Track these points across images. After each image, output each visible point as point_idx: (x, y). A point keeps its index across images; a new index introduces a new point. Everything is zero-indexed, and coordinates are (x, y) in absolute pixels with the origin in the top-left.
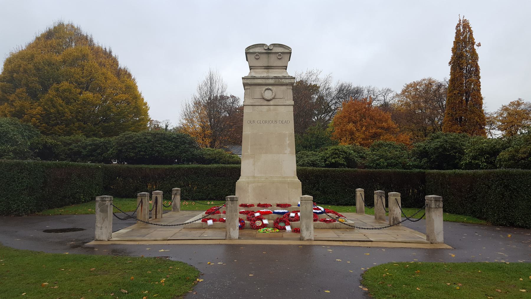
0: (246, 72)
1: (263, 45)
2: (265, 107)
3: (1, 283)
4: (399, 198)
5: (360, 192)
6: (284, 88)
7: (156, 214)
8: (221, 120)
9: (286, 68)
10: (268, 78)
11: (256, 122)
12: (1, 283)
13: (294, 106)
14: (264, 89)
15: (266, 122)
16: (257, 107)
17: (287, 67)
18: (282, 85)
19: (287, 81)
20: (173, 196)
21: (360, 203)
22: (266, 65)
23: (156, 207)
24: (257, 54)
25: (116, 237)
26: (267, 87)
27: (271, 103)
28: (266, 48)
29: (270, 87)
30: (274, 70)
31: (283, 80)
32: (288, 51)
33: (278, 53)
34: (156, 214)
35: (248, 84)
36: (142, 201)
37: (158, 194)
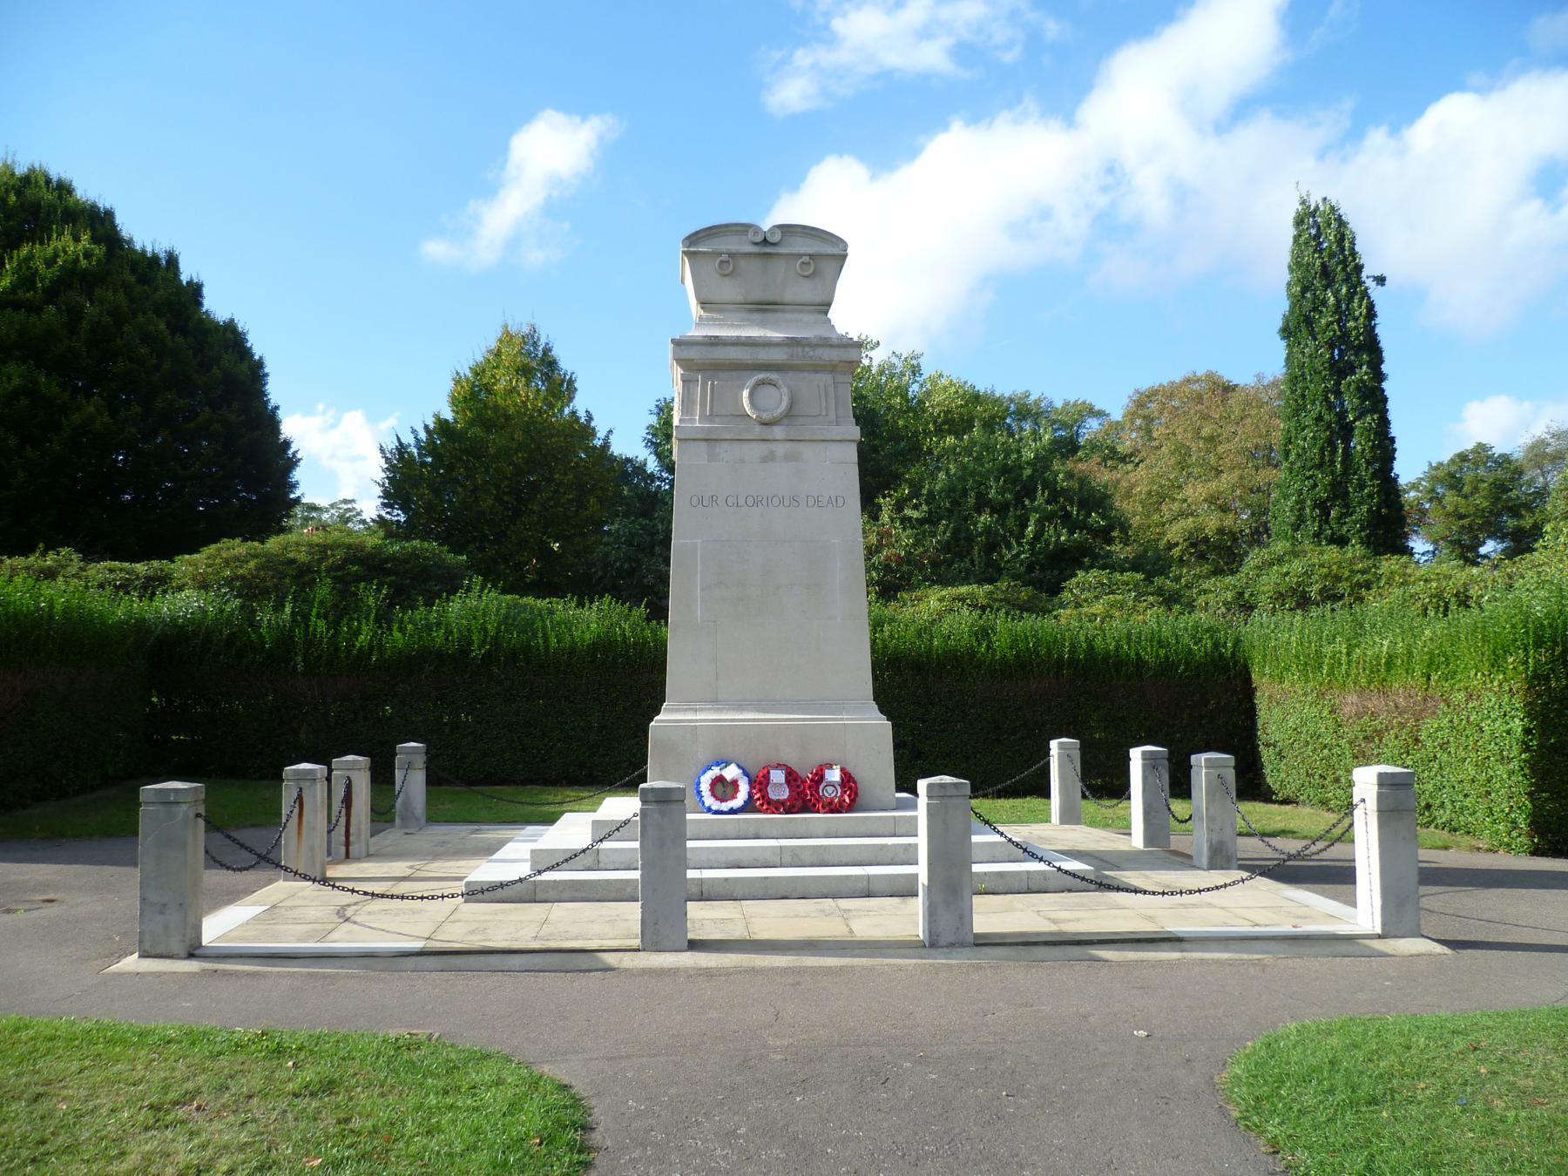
0: (691, 320)
1: (744, 229)
2: (754, 445)
3: (1564, 1112)
4: (1230, 775)
5: (1060, 752)
6: (825, 378)
7: (347, 844)
8: (514, 480)
9: (826, 306)
10: (767, 344)
12: (1564, 1112)
13: (860, 445)
14: (752, 381)
15: (756, 503)
16: (725, 445)
17: (829, 305)
18: (817, 368)
19: (827, 355)
20: (398, 774)
22: (758, 295)
23: (348, 815)
24: (725, 257)
25: (1098, 960)
26: (761, 376)
27: (778, 432)
28: (759, 238)
29: (773, 376)
30: (787, 316)
31: (819, 352)
32: (835, 251)
33: (801, 255)
34: (347, 844)
35: (702, 362)
36: (300, 799)
37: (353, 767)
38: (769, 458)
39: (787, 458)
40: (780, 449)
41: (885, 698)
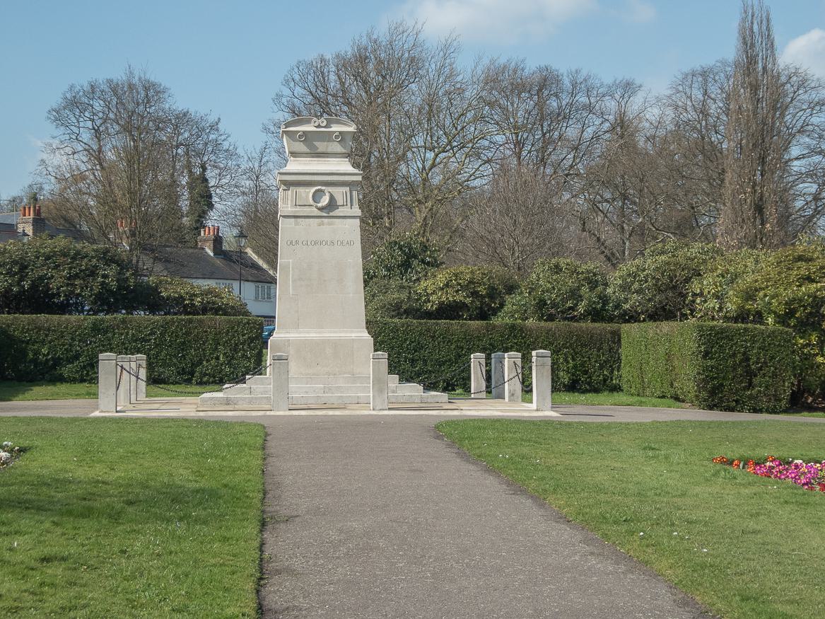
5: (476, 360)
11: (300, 243)
38: (323, 224)
41: (370, 325)
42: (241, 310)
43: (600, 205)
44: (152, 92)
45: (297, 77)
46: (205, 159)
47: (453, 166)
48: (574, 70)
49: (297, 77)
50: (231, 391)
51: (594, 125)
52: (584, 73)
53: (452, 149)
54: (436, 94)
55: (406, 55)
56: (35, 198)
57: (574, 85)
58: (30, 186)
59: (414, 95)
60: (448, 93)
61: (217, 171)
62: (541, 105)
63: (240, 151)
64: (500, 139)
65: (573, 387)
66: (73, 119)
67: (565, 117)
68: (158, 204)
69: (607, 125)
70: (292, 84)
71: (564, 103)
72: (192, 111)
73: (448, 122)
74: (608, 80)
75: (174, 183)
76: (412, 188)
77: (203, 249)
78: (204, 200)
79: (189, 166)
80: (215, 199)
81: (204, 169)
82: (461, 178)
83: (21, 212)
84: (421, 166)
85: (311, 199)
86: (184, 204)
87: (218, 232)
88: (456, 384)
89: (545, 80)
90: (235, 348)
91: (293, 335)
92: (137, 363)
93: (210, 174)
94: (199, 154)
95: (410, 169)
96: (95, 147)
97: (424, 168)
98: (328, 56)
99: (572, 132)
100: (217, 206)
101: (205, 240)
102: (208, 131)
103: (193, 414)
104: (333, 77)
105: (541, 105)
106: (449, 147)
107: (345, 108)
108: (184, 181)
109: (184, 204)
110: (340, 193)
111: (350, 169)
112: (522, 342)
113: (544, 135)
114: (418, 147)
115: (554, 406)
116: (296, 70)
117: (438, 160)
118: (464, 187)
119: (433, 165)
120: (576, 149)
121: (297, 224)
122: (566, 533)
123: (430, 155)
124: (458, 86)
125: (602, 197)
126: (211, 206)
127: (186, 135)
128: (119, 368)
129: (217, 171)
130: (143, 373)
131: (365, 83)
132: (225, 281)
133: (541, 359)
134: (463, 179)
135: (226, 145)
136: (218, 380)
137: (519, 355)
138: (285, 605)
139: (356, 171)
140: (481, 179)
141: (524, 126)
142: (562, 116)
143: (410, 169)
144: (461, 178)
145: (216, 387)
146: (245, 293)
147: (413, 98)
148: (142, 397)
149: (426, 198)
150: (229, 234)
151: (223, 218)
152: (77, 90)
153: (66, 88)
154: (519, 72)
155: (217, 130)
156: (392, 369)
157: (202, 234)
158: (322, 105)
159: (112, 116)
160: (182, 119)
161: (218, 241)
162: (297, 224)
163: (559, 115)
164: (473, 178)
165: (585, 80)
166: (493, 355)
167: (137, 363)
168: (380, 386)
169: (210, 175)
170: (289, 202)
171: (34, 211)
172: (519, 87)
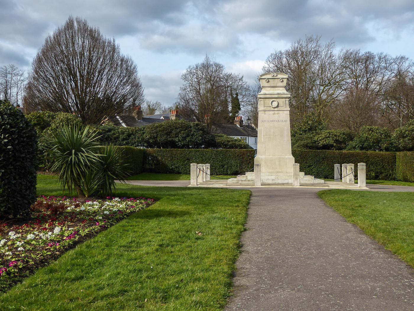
21: (337, 174)
38: (274, 114)
39: (278, 114)
40: (276, 112)
42: (247, 146)
43: (390, 106)
44: (219, 67)
45: (271, 60)
46: (237, 92)
47: (331, 92)
48: (380, 53)
49: (271, 60)
50: (240, 178)
51: (388, 75)
52: (384, 54)
53: (331, 85)
54: (325, 63)
55: (313, 49)
56: (177, 107)
57: (380, 58)
58: (176, 103)
59: (316, 66)
60: (329, 64)
61: (242, 96)
62: (366, 67)
63: (251, 89)
64: (349, 81)
65: (376, 177)
66: (190, 78)
67: (376, 72)
68: (220, 109)
69: (393, 75)
70: (269, 63)
71: (376, 66)
72: (233, 74)
73: (329, 75)
74: (394, 57)
75: (226, 100)
76: (314, 101)
77: (236, 125)
78: (237, 107)
79: (231, 94)
80: (241, 106)
81: (237, 95)
82: (335, 96)
83: (172, 112)
84: (318, 92)
85: (270, 104)
86: (230, 108)
87: (241, 119)
88: (329, 176)
89: (368, 58)
90: (245, 161)
91: (263, 157)
92: (206, 167)
93: (240, 97)
94: (236, 90)
95: (314, 93)
96: (198, 88)
97: (319, 93)
98: (283, 51)
99: (379, 78)
100: (242, 109)
101: (237, 122)
102: (238, 81)
103: (225, 186)
104: (285, 60)
105: (366, 67)
106: (329, 85)
107: (289, 71)
108: (229, 100)
109: (230, 108)
110: (281, 101)
111: (285, 92)
112: (354, 160)
113: (368, 79)
114: (317, 85)
115: (366, 186)
116: (270, 57)
117: (325, 90)
118: (334, 100)
119: (323, 91)
120: (380, 84)
121: (265, 114)
122: (364, 238)
123: (322, 88)
124: (333, 61)
125: (391, 103)
126: (240, 109)
127: (231, 83)
128: (198, 170)
129: (242, 96)
130: (209, 172)
131: (297, 61)
132: (244, 137)
133: (362, 167)
134: (335, 97)
135: (245, 86)
136: (236, 174)
137: (337, 166)
138: (241, 266)
139: (288, 93)
140: (340, 95)
141: (359, 76)
142: (375, 72)
143: (314, 93)
144: (335, 96)
145: (234, 176)
146: (250, 141)
147: (315, 66)
148: (208, 179)
149: (320, 104)
150: (244, 118)
151: (243, 114)
152: (191, 68)
153: (187, 67)
154: (357, 55)
155: (242, 80)
156: (301, 170)
157: (236, 119)
158: (279, 69)
159: (204, 76)
160: (229, 77)
161: (241, 122)
162: (265, 114)
163: (373, 71)
164: (339, 96)
165: (384, 57)
166: (343, 165)
167: (206, 167)
168: (296, 177)
169: (239, 97)
170: (262, 105)
171: (176, 112)
172: (357, 61)
